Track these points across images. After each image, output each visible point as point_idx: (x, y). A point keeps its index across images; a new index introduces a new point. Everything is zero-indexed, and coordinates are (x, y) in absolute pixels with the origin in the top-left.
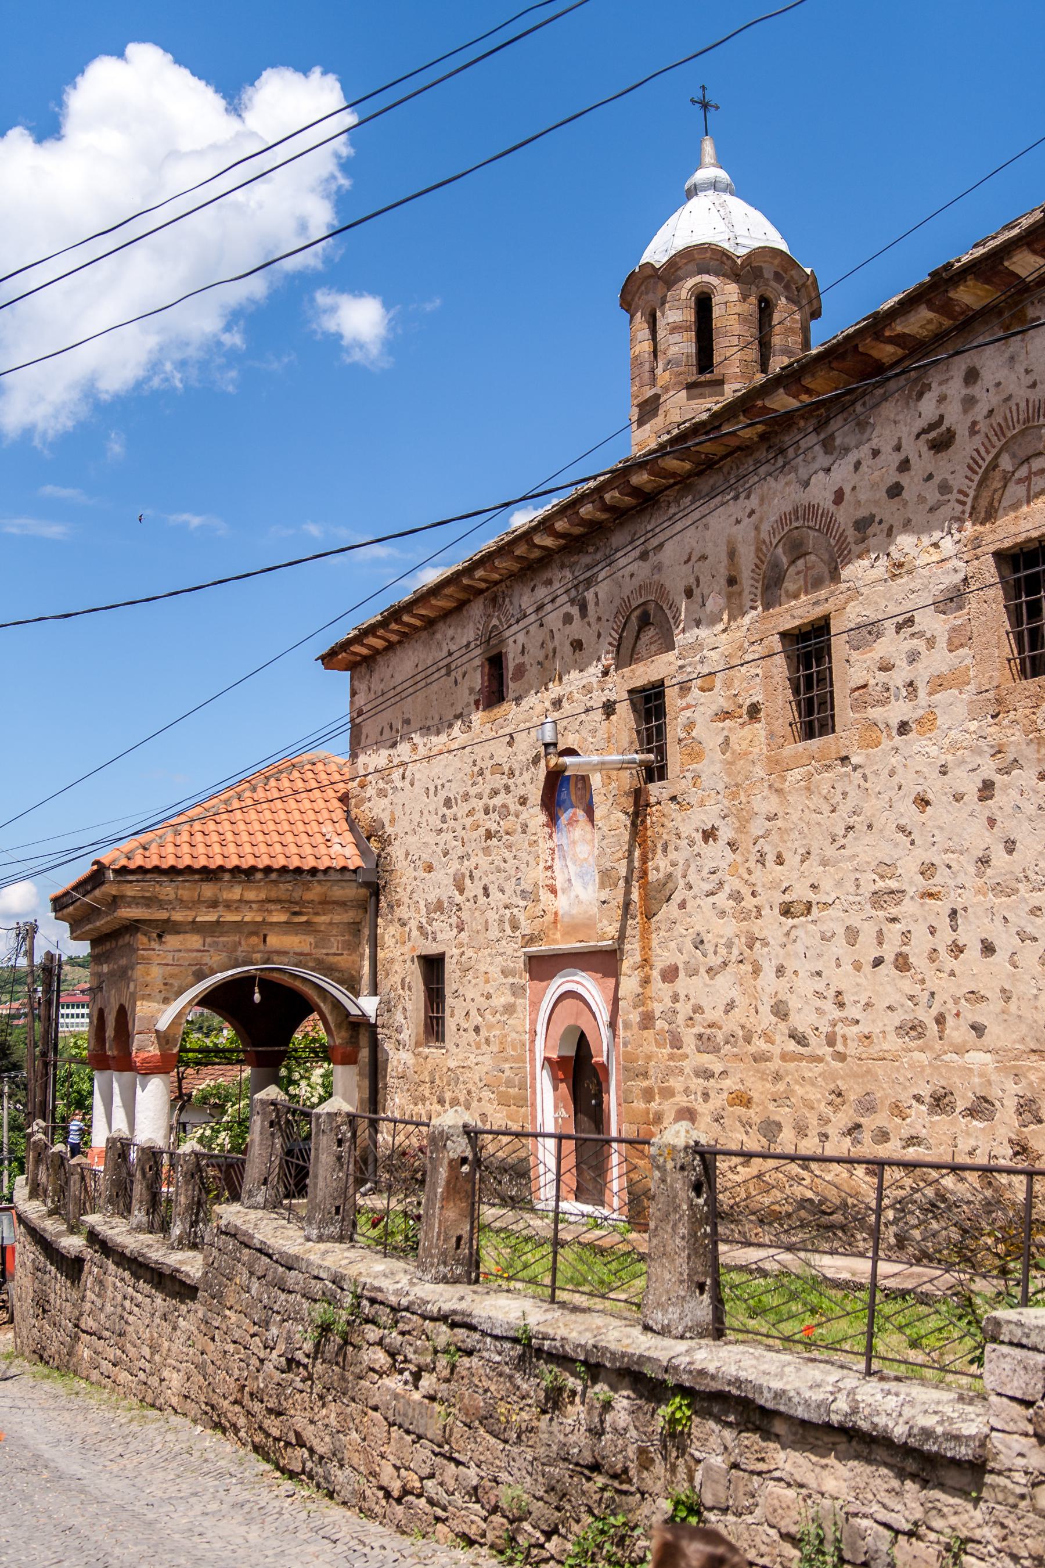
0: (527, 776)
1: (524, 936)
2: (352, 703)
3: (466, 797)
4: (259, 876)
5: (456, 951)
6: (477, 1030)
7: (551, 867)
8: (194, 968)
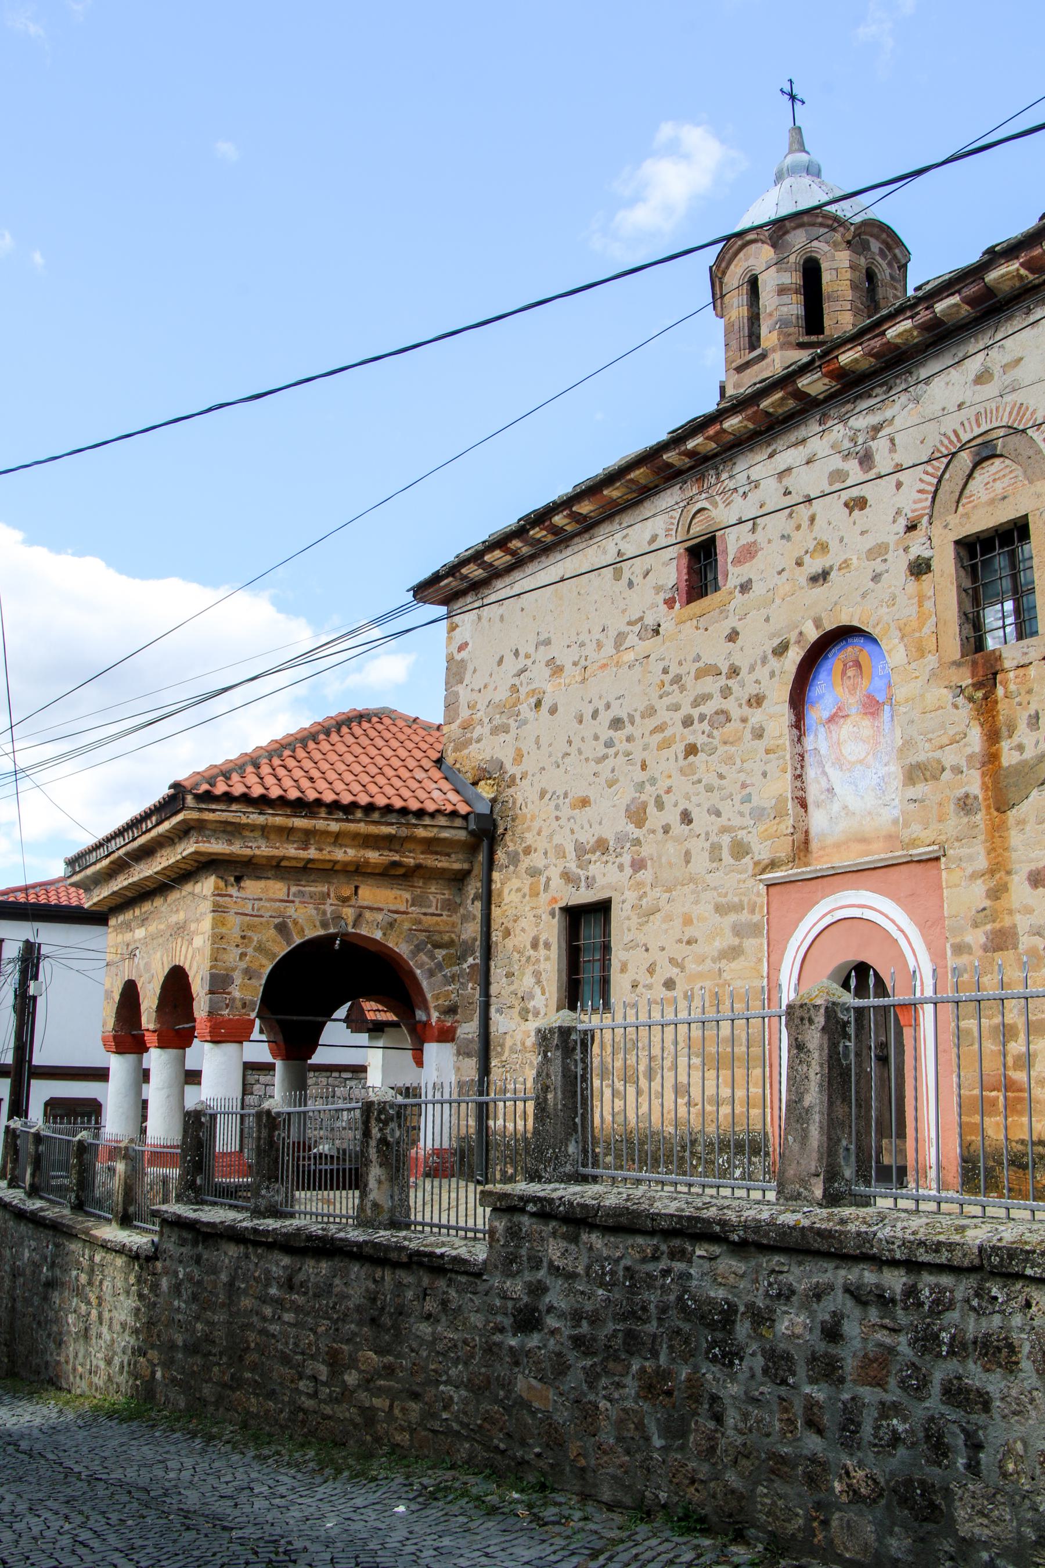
0: (762, 673)
1: (756, 864)
2: (450, 639)
3: (650, 711)
4: (359, 814)
5: (631, 896)
6: (669, 984)
7: (800, 776)
8: (277, 921)
